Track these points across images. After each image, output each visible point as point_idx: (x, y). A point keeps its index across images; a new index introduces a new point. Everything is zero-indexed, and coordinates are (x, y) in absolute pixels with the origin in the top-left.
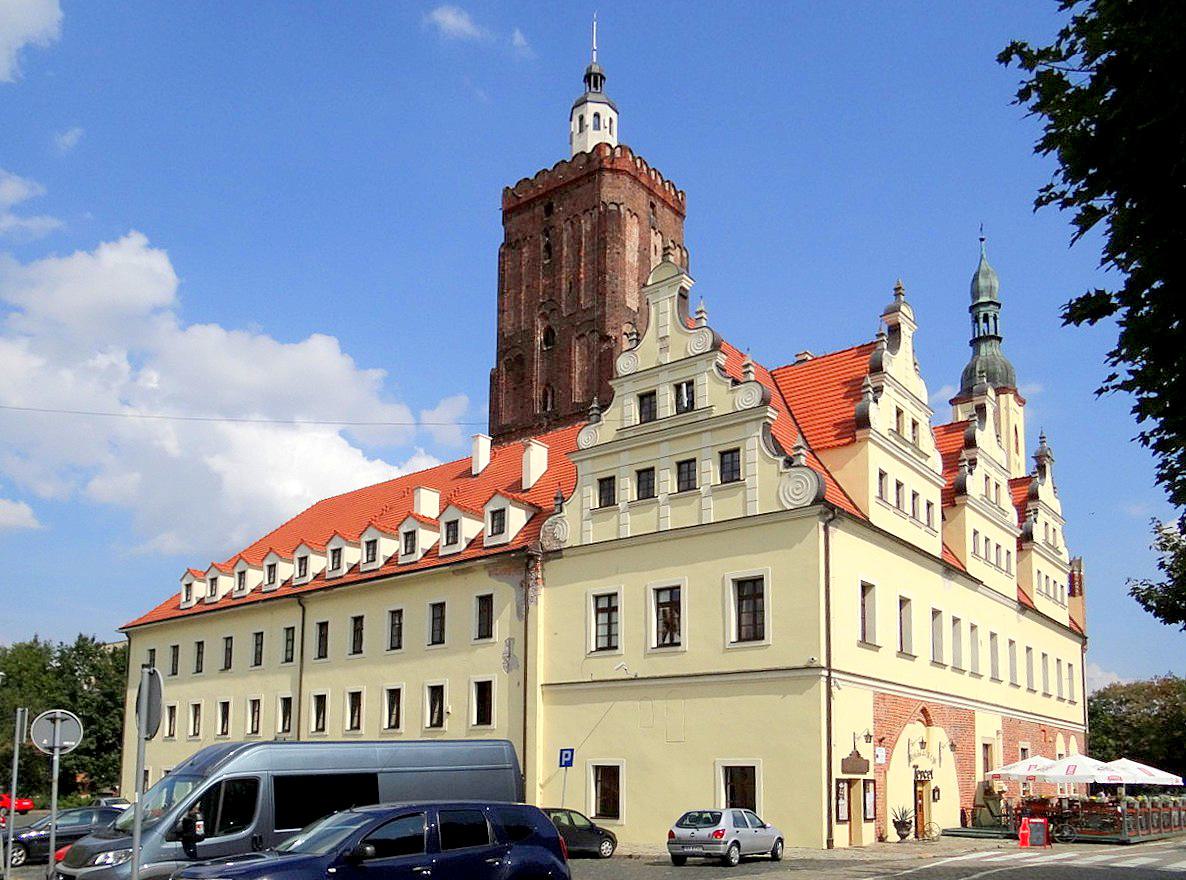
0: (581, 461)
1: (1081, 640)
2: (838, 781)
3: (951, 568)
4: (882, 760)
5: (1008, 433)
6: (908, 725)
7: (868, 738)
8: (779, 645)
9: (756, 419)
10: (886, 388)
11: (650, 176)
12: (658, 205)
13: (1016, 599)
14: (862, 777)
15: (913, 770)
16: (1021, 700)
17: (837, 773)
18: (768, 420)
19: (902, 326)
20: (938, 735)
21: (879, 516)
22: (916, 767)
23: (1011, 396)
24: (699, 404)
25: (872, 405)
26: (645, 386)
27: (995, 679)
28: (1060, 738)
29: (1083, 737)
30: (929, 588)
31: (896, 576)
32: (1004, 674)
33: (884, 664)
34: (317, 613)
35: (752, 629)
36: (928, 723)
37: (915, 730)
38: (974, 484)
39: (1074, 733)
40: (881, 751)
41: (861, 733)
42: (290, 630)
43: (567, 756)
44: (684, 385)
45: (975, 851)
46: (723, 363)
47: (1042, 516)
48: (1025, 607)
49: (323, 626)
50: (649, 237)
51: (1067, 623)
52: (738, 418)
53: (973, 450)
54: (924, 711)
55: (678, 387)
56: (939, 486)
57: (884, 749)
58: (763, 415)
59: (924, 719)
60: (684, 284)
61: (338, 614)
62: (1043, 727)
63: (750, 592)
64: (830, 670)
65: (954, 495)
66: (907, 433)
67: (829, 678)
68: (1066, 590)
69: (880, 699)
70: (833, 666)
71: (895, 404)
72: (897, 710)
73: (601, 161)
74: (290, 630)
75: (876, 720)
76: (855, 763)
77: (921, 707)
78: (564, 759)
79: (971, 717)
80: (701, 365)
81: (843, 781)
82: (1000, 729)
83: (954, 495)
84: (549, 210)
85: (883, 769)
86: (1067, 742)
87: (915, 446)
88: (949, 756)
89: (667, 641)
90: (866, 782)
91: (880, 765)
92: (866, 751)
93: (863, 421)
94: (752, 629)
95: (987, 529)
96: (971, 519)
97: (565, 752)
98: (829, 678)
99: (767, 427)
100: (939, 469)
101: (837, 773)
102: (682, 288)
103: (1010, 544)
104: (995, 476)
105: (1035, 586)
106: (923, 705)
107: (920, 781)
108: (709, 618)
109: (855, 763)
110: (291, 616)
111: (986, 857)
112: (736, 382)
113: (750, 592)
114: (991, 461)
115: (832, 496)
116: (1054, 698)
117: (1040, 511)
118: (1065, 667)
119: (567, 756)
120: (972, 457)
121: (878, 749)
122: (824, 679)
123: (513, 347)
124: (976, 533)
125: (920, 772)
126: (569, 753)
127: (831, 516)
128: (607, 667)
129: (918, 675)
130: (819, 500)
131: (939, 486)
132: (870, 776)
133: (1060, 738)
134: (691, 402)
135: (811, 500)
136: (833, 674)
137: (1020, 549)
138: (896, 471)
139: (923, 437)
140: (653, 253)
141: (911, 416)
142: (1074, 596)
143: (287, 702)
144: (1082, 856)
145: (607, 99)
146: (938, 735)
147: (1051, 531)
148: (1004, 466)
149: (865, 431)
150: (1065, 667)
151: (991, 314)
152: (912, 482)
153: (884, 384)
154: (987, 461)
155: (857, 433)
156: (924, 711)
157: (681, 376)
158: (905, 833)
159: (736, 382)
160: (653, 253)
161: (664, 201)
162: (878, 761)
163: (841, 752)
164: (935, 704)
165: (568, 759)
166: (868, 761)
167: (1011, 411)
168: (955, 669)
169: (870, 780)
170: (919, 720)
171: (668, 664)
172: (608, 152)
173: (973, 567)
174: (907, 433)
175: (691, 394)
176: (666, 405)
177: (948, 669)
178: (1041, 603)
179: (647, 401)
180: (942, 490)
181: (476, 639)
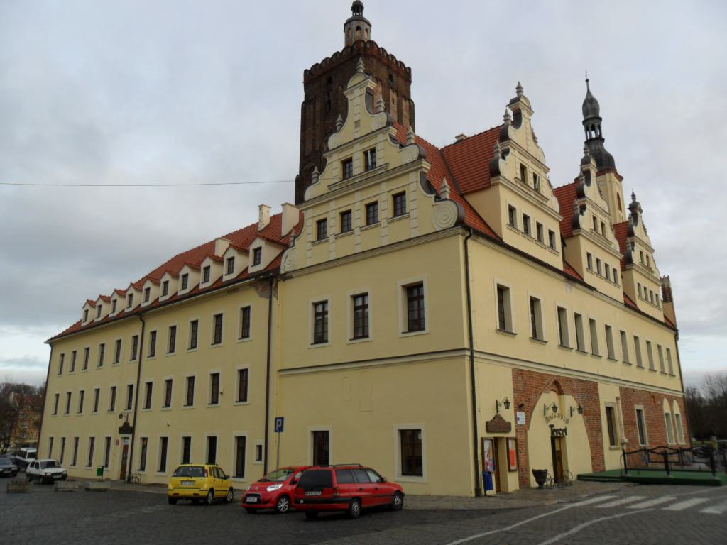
0: (306, 209)
1: (673, 332)
2: (483, 440)
3: (571, 276)
4: (522, 421)
5: (613, 197)
6: (543, 394)
7: (507, 404)
8: (433, 337)
9: (414, 170)
10: (511, 151)
11: (389, 59)
12: (394, 76)
13: (623, 302)
14: (505, 435)
15: (549, 429)
16: (635, 376)
17: (482, 432)
18: (423, 170)
19: (522, 111)
20: (570, 401)
21: (509, 237)
22: (551, 426)
23: (613, 175)
24: (379, 163)
25: (501, 161)
26: (345, 155)
27: (652, 370)
28: (666, 402)
29: (682, 401)
30: (555, 293)
31: (525, 283)
32: (657, 367)
33: (520, 347)
34: (151, 326)
35: (415, 323)
36: (560, 392)
37: (549, 398)
38: (585, 222)
39: (676, 398)
40: (521, 415)
41: (502, 400)
42: (136, 338)
43: (279, 422)
44: (369, 152)
45: (597, 495)
46: (394, 135)
47: (637, 248)
48: (630, 305)
49: (154, 333)
50: (389, 94)
51: (662, 320)
52: (404, 170)
53: (582, 199)
54: (556, 383)
55: (366, 153)
56: (558, 220)
57: (523, 413)
58: (420, 166)
59: (557, 389)
60: (369, 86)
61: (161, 325)
62: (652, 394)
63: (414, 293)
64: (472, 351)
65: (570, 228)
66: (530, 181)
67: (472, 357)
68: (661, 297)
69: (518, 374)
70: (474, 349)
71: (519, 161)
72: (529, 385)
73: (359, 50)
74: (136, 338)
75: (515, 390)
76: (497, 424)
77: (553, 380)
78: (278, 426)
79: (595, 386)
80: (380, 137)
81: (487, 439)
82: (618, 395)
83: (570, 228)
84: (330, 81)
85: (523, 429)
86: (671, 404)
87: (537, 190)
88: (579, 419)
89: (360, 335)
90: (507, 439)
91: (521, 425)
92: (508, 415)
93: (495, 172)
94: (415, 323)
95: (597, 253)
96: (585, 246)
97: (278, 420)
98: (472, 357)
99: (423, 174)
100: (618, 250)
101: (482, 432)
102: (368, 88)
103: (615, 264)
104: (600, 218)
105: (637, 293)
106: (555, 378)
107: (557, 437)
108: (388, 314)
109: (497, 424)
110: (135, 329)
111: (602, 502)
112: (402, 146)
113: (414, 293)
114: (596, 207)
115: (470, 220)
116: (658, 373)
117: (636, 244)
118: (664, 352)
119: (279, 422)
120: (582, 203)
121: (518, 413)
122: (467, 358)
123: (309, 162)
124: (589, 255)
125: (556, 430)
126: (280, 420)
127: (468, 234)
128: (323, 354)
129: (549, 356)
130: (460, 222)
131: (558, 220)
132: (513, 434)
133: (666, 402)
134: (374, 163)
135: (453, 224)
136: (475, 355)
137: (623, 269)
138: (597, 253)
139: (542, 181)
140: (391, 103)
141: (532, 171)
142: (667, 302)
143: (131, 387)
144: (680, 499)
145: (665, 317)
146: (570, 401)
147: (645, 257)
148: (607, 211)
149: (496, 178)
150: (664, 352)
151: (597, 124)
152: (536, 216)
153: (509, 147)
154: (593, 207)
155: (491, 180)
156: (556, 383)
157: (367, 145)
158: (542, 480)
159: (402, 146)
160: (391, 103)
161: (397, 72)
162: (519, 422)
163: (485, 416)
164: (565, 378)
165: (280, 426)
166: (510, 423)
167: (614, 184)
168: (593, 355)
169: (512, 439)
170: (553, 390)
171: (362, 350)
172: (362, 45)
173: (589, 278)
174: (530, 181)
175: (373, 157)
176: (358, 167)
177: (574, 351)
178: (641, 305)
179: (347, 163)
180: (560, 222)
181: (312, 344)
